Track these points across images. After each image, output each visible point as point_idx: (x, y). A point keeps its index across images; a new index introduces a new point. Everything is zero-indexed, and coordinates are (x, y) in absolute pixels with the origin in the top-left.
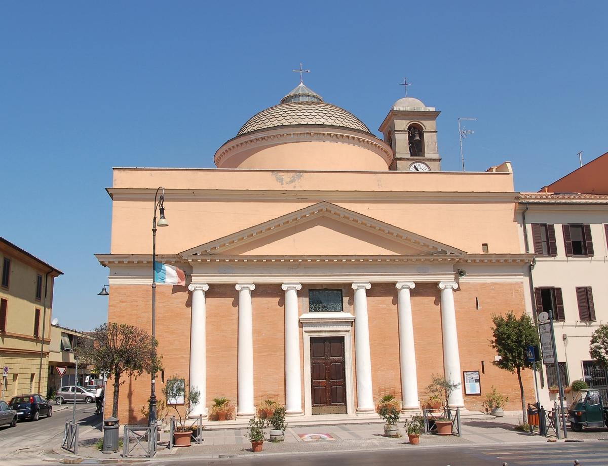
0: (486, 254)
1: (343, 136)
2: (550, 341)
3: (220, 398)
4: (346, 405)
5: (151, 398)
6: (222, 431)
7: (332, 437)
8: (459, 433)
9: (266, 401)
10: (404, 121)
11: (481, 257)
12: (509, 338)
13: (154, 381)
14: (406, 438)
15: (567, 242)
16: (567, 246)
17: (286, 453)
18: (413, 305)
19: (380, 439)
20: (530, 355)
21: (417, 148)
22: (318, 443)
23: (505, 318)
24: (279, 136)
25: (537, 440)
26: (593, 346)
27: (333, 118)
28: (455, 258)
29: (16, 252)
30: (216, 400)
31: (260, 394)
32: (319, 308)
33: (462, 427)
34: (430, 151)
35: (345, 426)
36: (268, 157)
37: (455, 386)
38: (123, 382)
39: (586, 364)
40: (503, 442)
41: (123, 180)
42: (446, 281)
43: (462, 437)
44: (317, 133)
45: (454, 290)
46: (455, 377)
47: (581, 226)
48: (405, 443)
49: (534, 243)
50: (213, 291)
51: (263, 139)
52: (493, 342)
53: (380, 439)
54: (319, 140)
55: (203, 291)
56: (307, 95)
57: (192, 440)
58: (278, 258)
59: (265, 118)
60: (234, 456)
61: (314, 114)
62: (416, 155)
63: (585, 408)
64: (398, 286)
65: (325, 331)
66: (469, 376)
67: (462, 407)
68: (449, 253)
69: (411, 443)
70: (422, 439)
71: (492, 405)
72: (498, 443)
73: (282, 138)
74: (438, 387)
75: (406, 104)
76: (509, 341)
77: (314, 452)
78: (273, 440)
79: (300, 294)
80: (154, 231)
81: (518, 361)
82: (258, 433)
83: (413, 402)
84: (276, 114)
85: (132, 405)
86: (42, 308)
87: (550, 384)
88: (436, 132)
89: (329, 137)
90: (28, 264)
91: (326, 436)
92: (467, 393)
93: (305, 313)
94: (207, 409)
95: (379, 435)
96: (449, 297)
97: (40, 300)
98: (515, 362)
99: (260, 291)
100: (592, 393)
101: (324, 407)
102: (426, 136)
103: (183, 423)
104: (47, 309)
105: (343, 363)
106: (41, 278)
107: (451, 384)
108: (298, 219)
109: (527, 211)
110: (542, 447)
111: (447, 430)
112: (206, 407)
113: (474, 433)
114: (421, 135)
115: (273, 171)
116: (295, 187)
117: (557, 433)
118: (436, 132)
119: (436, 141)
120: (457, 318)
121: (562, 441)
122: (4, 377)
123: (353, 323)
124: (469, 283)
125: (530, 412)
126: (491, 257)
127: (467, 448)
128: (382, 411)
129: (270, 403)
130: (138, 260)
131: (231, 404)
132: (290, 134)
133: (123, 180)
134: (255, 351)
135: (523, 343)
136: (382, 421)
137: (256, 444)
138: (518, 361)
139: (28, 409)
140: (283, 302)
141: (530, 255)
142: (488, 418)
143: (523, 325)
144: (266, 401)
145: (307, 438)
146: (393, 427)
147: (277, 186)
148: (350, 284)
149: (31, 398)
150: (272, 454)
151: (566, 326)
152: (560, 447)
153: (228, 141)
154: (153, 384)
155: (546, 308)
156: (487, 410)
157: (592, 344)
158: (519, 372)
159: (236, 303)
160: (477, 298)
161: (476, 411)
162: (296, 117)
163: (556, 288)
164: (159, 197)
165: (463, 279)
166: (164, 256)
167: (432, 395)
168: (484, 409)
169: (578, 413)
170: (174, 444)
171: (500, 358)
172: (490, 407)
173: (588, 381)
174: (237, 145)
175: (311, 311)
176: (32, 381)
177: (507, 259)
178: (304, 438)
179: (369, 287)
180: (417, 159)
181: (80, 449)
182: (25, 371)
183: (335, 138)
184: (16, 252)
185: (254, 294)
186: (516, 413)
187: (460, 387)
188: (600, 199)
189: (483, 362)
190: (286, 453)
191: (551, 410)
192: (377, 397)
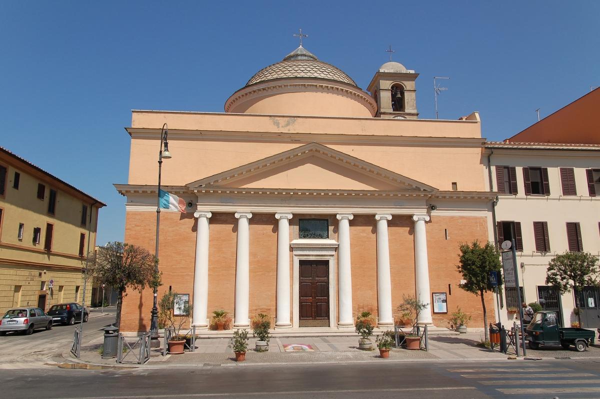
0: (455, 191)
1: (333, 88)
2: (512, 267)
3: (220, 311)
4: (329, 320)
5: (153, 310)
6: (218, 340)
7: (312, 349)
8: (426, 348)
9: (259, 315)
10: (388, 81)
11: (451, 194)
12: (474, 264)
13: (156, 295)
14: (377, 352)
15: (526, 182)
16: (526, 186)
17: (265, 364)
18: (390, 234)
19: (354, 351)
20: (493, 280)
21: (398, 104)
22: (298, 354)
23: (471, 246)
24: (278, 87)
25: (497, 357)
26: (549, 273)
27: (325, 73)
28: (428, 194)
29: (61, 185)
30: (215, 313)
31: (255, 308)
32: (308, 235)
33: (429, 341)
34: (409, 109)
35: (326, 338)
36: (269, 105)
37: (424, 306)
38: (126, 295)
39: (540, 289)
40: (467, 358)
41: (140, 121)
42: (419, 214)
43: (430, 351)
44: (311, 85)
45: (426, 222)
46: (425, 298)
47: (540, 169)
48: (376, 357)
49: (497, 183)
50: (215, 218)
51: (264, 89)
52: (459, 267)
53: (354, 351)
54: (313, 91)
55: (207, 218)
56: (305, 55)
57: (185, 348)
58: (272, 191)
59: (267, 73)
60: (217, 365)
61: (308, 69)
62: (397, 110)
63: (542, 328)
64: (377, 217)
65: (312, 256)
66: (437, 297)
67: (431, 324)
68: (422, 190)
69: (381, 356)
70: (392, 353)
71: (457, 323)
72: (462, 359)
73: (280, 89)
74: (409, 306)
75: (391, 67)
76: (473, 267)
77: (291, 363)
78: (258, 349)
79: (291, 222)
80: (160, 162)
81: (482, 285)
82: (242, 344)
83: (388, 317)
84: (276, 69)
85: (143, 315)
86: (86, 232)
87: (508, 305)
88: (415, 91)
89: (321, 89)
90: (74, 196)
91: (307, 347)
92: (435, 311)
93: (295, 239)
94: (208, 319)
95: (354, 347)
96: (421, 228)
97: (85, 226)
98: (479, 286)
99: (256, 219)
100: (549, 315)
101: (310, 321)
102: (406, 94)
103: (177, 332)
104: (91, 233)
105: (328, 283)
106: (86, 209)
107: (420, 304)
108: (291, 157)
109: (492, 155)
110: (503, 365)
111: (416, 345)
112: (207, 318)
113: (440, 348)
114: (402, 94)
115: (270, 116)
116: (289, 130)
117: (517, 351)
118: (415, 91)
119: (415, 98)
120: (428, 247)
121: (521, 358)
122: (49, 288)
123: (337, 249)
124: (439, 216)
125: (492, 331)
126: (460, 194)
127: (432, 364)
128: (359, 326)
129: (263, 316)
130: (150, 190)
131: (229, 316)
132: (287, 86)
133: (140, 121)
134: (251, 271)
135: (487, 268)
136: (357, 334)
137: (240, 354)
138: (482, 285)
139: (65, 315)
140: (276, 229)
141: (494, 194)
142: (452, 334)
143: (487, 252)
144: (259, 315)
145: (289, 349)
146: (367, 342)
147: (273, 129)
148: (335, 215)
149: (68, 306)
150: (253, 364)
151: (524, 256)
152: (520, 365)
153: (236, 92)
154: (155, 297)
155: (507, 237)
156: (452, 326)
157: (549, 271)
158: (482, 295)
159: (236, 229)
160: (446, 230)
161: (442, 327)
162: (293, 71)
163: (516, 223)
164: (164, 135)
165: (434, 213)
166: (174, 187)
167: (403, 313)
168: (450, 326)
169: (536, 333)
170: (169, 351)
171: (465, 281)
172: (455, 324)
173: (541, 303)
174: (243, 96)
175: (300, 238)
176: (77, 291)
177: (473, 196)
178: (287, 348)
179: (351, 217)
180: (398, 114)
181: (82, 353)
182: (70, 284)
183: (326, 89)
184: (61, 185)
185: (251, 221)
186: (478, 330)
187: (429, 307)
188: (557, 146)
189: (449, 285)
190: (265, 364)
191: (511, 330)
192: (356, 313)
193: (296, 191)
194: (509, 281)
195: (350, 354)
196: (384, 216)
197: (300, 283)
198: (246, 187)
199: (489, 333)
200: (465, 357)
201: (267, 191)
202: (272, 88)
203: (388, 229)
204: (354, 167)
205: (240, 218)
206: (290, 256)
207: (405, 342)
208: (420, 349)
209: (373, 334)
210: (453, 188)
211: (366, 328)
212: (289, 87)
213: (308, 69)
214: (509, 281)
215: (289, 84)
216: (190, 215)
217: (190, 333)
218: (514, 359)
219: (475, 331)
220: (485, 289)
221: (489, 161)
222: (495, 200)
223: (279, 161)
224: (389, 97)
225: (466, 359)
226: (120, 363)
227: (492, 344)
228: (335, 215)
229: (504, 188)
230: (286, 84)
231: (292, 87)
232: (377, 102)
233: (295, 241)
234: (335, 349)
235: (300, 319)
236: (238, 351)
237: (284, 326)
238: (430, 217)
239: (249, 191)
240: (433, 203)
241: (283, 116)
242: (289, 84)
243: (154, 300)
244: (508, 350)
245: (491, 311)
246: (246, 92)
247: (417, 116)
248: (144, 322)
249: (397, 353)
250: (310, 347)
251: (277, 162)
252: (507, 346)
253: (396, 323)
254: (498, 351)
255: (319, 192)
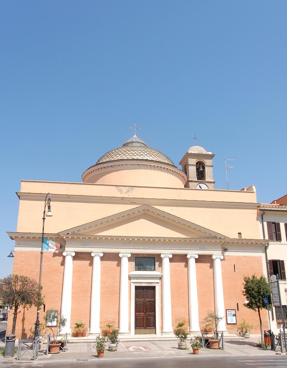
1: (158, 167)
2: (277, 292)
3: (79, 323)
4: (155, 329)
5: (37, 322)
7: (146, 349)
8: (223, 348)
9: (107, 325)
10: (194, 159)
11: (247, 241)
12: (253, 290)
13: (39, 311)
14: (191, 350)
17: (118, 359)
18: (197, 268)
20: (266, 301)
21: (201, 175)
22: (138, 352)
24: (121, 165)
27: (153, 156)
30: (76, 324)
31: (104, 321)
32: (141, 269)
33: (225, 344)
36: (115, 177)
37: (221, 319)
40: (249, 354)
41: (26, 188)
42: (217, 254)
43: (225, 350)
44: (143, 165)
45: (221, 260)
46: (221, 313)
48: (191, 354)
50: (78, 256)
51: (111, 166)
52: (243, 292)
54: (144, 169)
55: (72, 256)
57: (61, 349)
58: (117, 238)
61: (146, 154)
62: (200, 179)
64: (188, 256)
65: (144, 283)
66: (230, 313)
67: (225, 331)
68: (218, 238)
69: (194, 353)
71: (243, 331)
73: (122, 166)
74: (211, 319)
75: (195, 149)
76: (253, 292)
78: (110, 350)
79: (130, 259)
80: (44, 219)
81: (258, 304)
82: (101, 346)
87: (277, 319)
91: (143, 348)
92: (228, 323)
93: (133, 271)
94: (71, 329)
95: (175, 348)
96: (218, 264)
98: (257, 305)
99: (106, 257)
102: (206, 168)
103: (55, 338)
105: (154, 302)
107: (219, 317)
109: (264, 215)
111: (216, 346)
112: (70, 328)
113: (232, 348)
114: (204, 168)
115: (116, 186)
116: (129, 196)
117: (281, 349)
119: (212, 171)
123: (161, 278)
125: (266, 336)
126: (243, 241)
127: (228, 358)
128: (177, 333)
129: (109, 326)
132: (127, 165)
133: (26, 188)
137: (100, 352)
138: (258, 304)
140: (119, 264)
141: (266, 241)
142: (241, 339)
143: (261, 282)
144: (107, 325)
145: (131, 349)
146: (183, 343)
147: (118, 195)
148: (160, 255)
153: (91, 167)
154: (38, 313)
158: (259, 311)
159: (91, 264)
160: (234, 265)
161: (233, 334)
162: (131, 155)
164: (48, 198)
165: (226, 254)
167: (207, 323)
168: (238, 333)
170: (49, 352)
171: (248, 302)
172: (242, 332)
174: (96, 170)
177: (262, 242)
178: (129, 349)
179: (171, 256)
180: (201, 182)
185: (102, 259)
187: (224, 319)
189: (238, 304)
190: (118, 359)
191: (278, 335)
193: (134, 238)
194: (276, 302)
195: (173, 352)
196: (97, 254)
197: (136, 302)
198: (99, 235)
199: (264, 338)
200: (248, 353)
201: (86, 237)
202: (117, 166)
203: (196, 265)
204: (173, 221)
205: (94, 256)
206: (129, 283)
207: (209, 344)
208: (219, 349)
209: (188, 338)
210: (239, 237)
211: (183, 334)
212: (128, 165)
213: (146, 154)
214: (276, 302)
215: (128, 164)
216: (60, 254)
217: (63, 339)
218: (279, 354)
219: (255, 337)
220: (261, 307)
221: (262, 219)
222: (267, 245)
223: (122, 217)
224: (195, 170)
225: (249, 355)
226: (19, 359)
227: (266, 344)
228: (160, 255)
229: (273, 235)
230: (126, 164)
231: (131, 166)
232: (186, 173)
233: (131, 273)
234: (162, 349)
235: (135, 329)
236: (99, 350)
237: (124, 333)
238: (224, 256)
239: (101, 237)
240: (226, 247)
241: (125, 186)
242: (128, 164)
243: (37, 315)
244: (276, 349)
245: (266, 322)
246: (98, 168)
247: (217, 186)
248: (26, 332)
249: (204, 351)
250: (144, 347)
251: (121, 217)
252: (276, 346)
253: (202, 331)
254: (270, 349)
255: (149, 239)
